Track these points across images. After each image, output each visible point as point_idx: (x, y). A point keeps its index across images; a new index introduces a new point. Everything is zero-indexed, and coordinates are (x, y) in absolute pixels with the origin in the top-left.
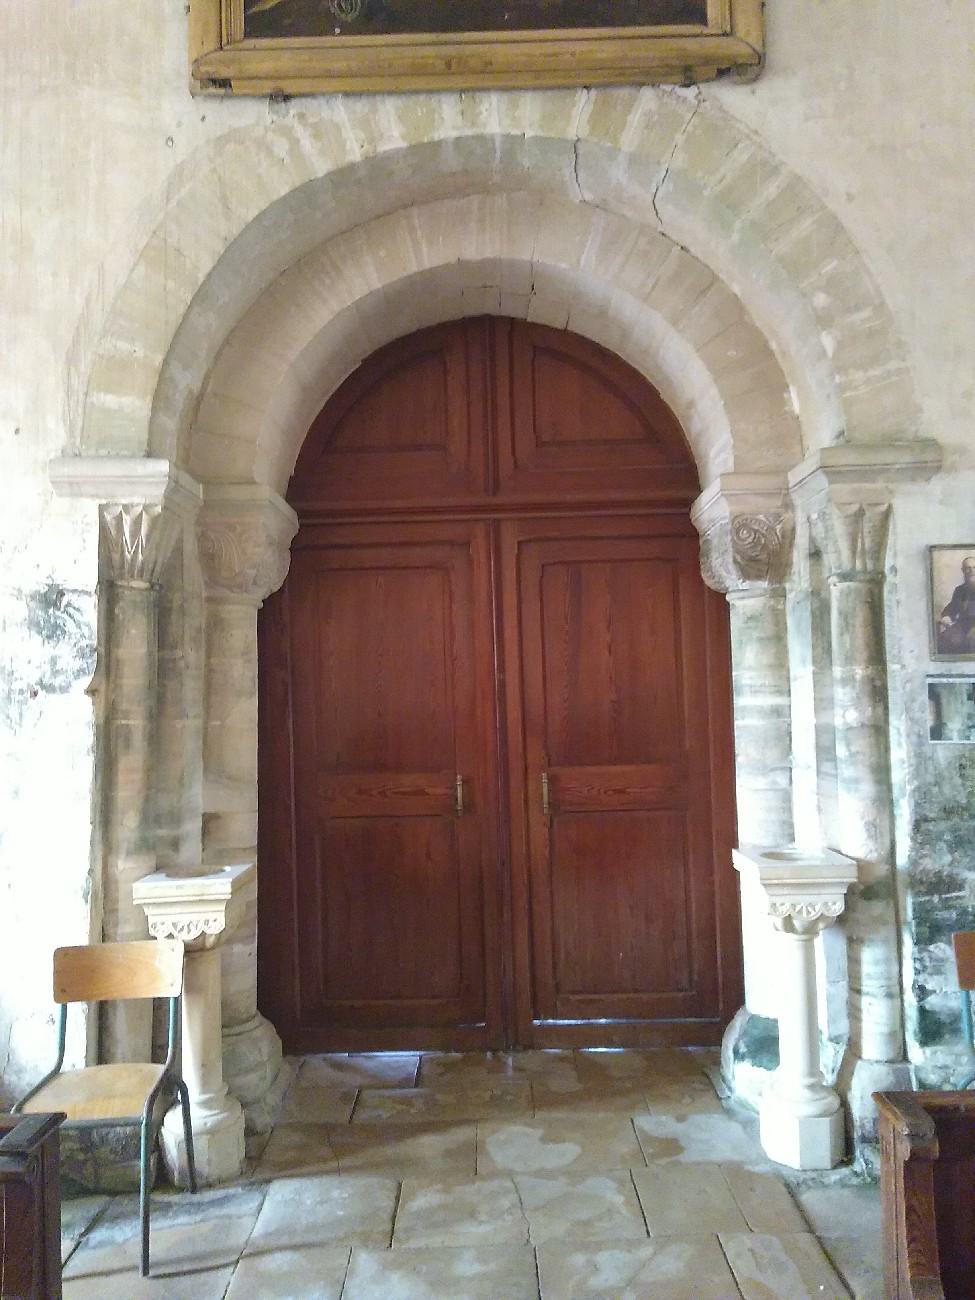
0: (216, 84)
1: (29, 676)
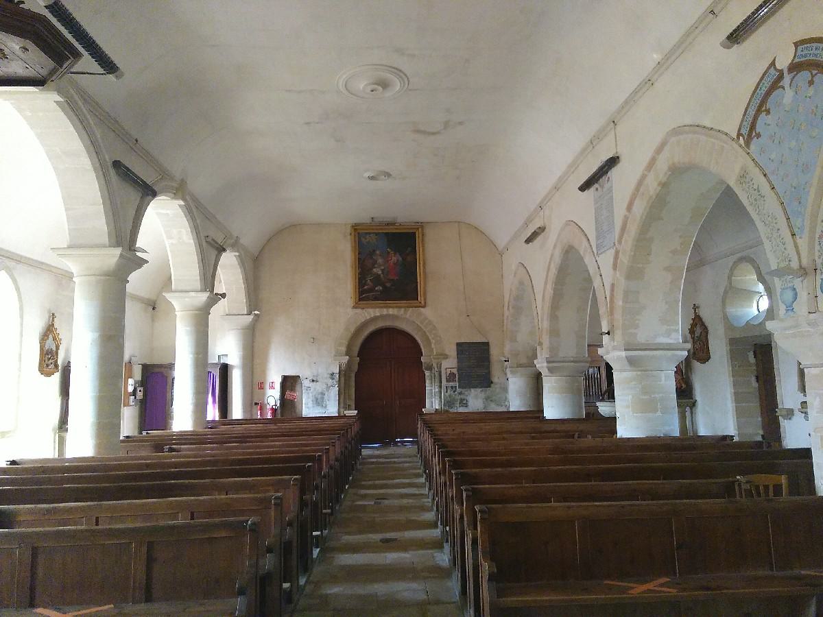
0: (354, 307)
1: (329, 384)
